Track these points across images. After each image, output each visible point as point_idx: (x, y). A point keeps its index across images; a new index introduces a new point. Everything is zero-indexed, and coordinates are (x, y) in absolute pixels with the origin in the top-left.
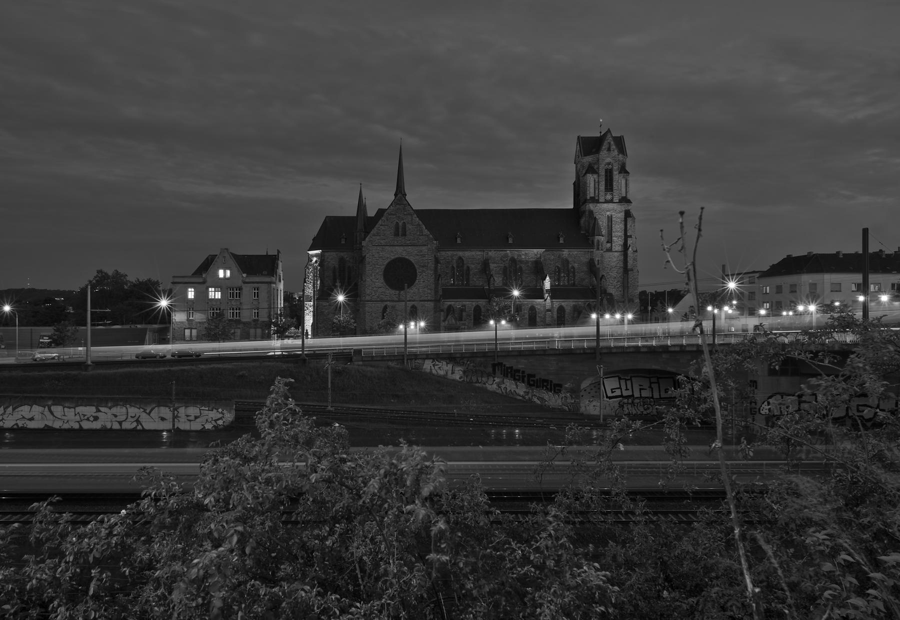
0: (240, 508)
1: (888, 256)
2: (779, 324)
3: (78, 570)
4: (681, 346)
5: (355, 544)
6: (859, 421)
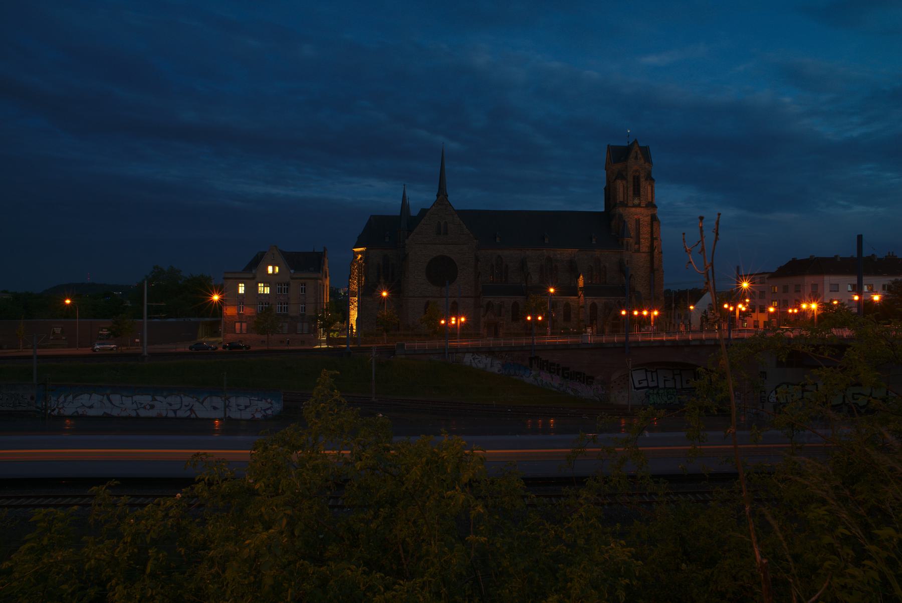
1: (879, 260)
3: (136, 550)
4: (701, 340)
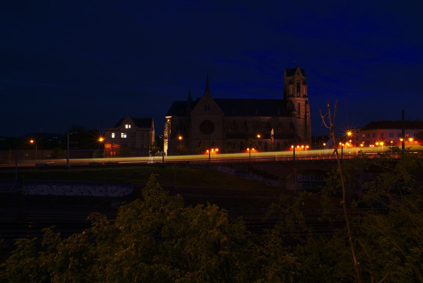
0: (135, 231)
2: (368, 150)
4: (329, 160)
5: (187, 247)
6: (401, 192)
